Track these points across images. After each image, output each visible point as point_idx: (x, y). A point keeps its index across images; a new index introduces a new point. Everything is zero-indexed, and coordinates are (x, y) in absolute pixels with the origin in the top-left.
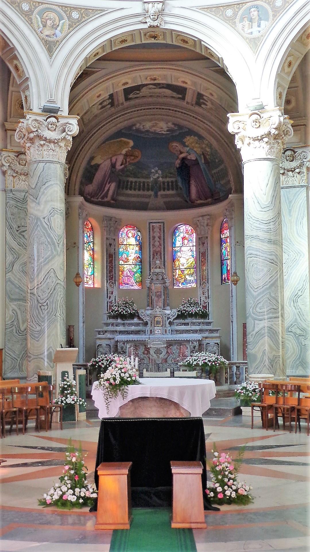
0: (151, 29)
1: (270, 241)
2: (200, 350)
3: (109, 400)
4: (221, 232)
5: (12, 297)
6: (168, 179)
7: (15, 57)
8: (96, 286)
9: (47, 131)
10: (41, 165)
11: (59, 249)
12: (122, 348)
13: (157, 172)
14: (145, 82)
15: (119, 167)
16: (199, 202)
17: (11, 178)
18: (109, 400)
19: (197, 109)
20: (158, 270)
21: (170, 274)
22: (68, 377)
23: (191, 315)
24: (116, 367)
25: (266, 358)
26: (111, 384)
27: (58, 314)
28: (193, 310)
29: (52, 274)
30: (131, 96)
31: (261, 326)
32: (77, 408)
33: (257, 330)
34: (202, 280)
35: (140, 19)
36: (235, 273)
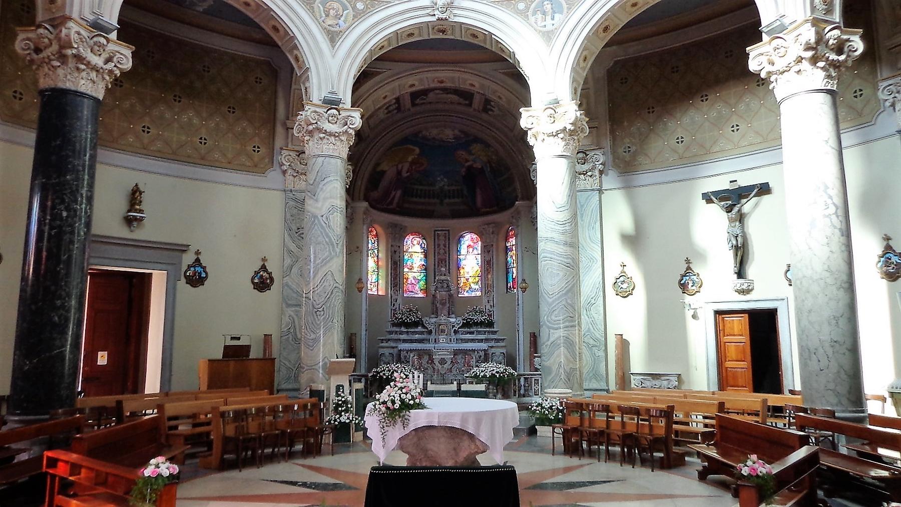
0: (442, 23)
1: (566, 244)
2: (486, 360)
3: (386, 428)
4: (507, 240)
5: (290, 302)
6: (453, 188)
7: (295, 47)
8: (380, 293)
9: (328, 124)
10: (320, 159)
11: (338, 250)
12: (405, 357)
13: (442, 180)
14: (433, 85)
15: (405, 174)
16: (484, 210)
17: (291, 177)
18: (386, 428)
19: (484, 116)
20: (443, 278)
21: (455, 282)
22: (343, 392)
23: (476, 324)
24: (396, 386)
25: (562, 371)
26: (388, 408)
27: (335, 321)
28: (479, 318)
29: (329, 277)
30: (418, 101)
31: (556, 336)
32: (353, 426)
33: (552, 339)
34: (487, 288)
35: (428, 11)
36: (524, 280)
